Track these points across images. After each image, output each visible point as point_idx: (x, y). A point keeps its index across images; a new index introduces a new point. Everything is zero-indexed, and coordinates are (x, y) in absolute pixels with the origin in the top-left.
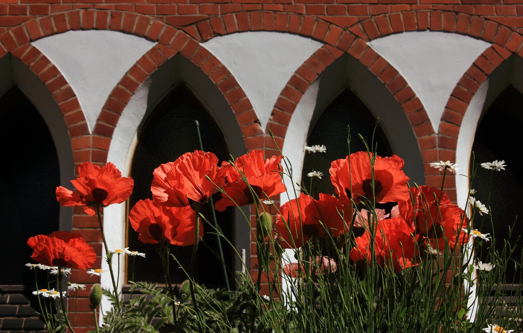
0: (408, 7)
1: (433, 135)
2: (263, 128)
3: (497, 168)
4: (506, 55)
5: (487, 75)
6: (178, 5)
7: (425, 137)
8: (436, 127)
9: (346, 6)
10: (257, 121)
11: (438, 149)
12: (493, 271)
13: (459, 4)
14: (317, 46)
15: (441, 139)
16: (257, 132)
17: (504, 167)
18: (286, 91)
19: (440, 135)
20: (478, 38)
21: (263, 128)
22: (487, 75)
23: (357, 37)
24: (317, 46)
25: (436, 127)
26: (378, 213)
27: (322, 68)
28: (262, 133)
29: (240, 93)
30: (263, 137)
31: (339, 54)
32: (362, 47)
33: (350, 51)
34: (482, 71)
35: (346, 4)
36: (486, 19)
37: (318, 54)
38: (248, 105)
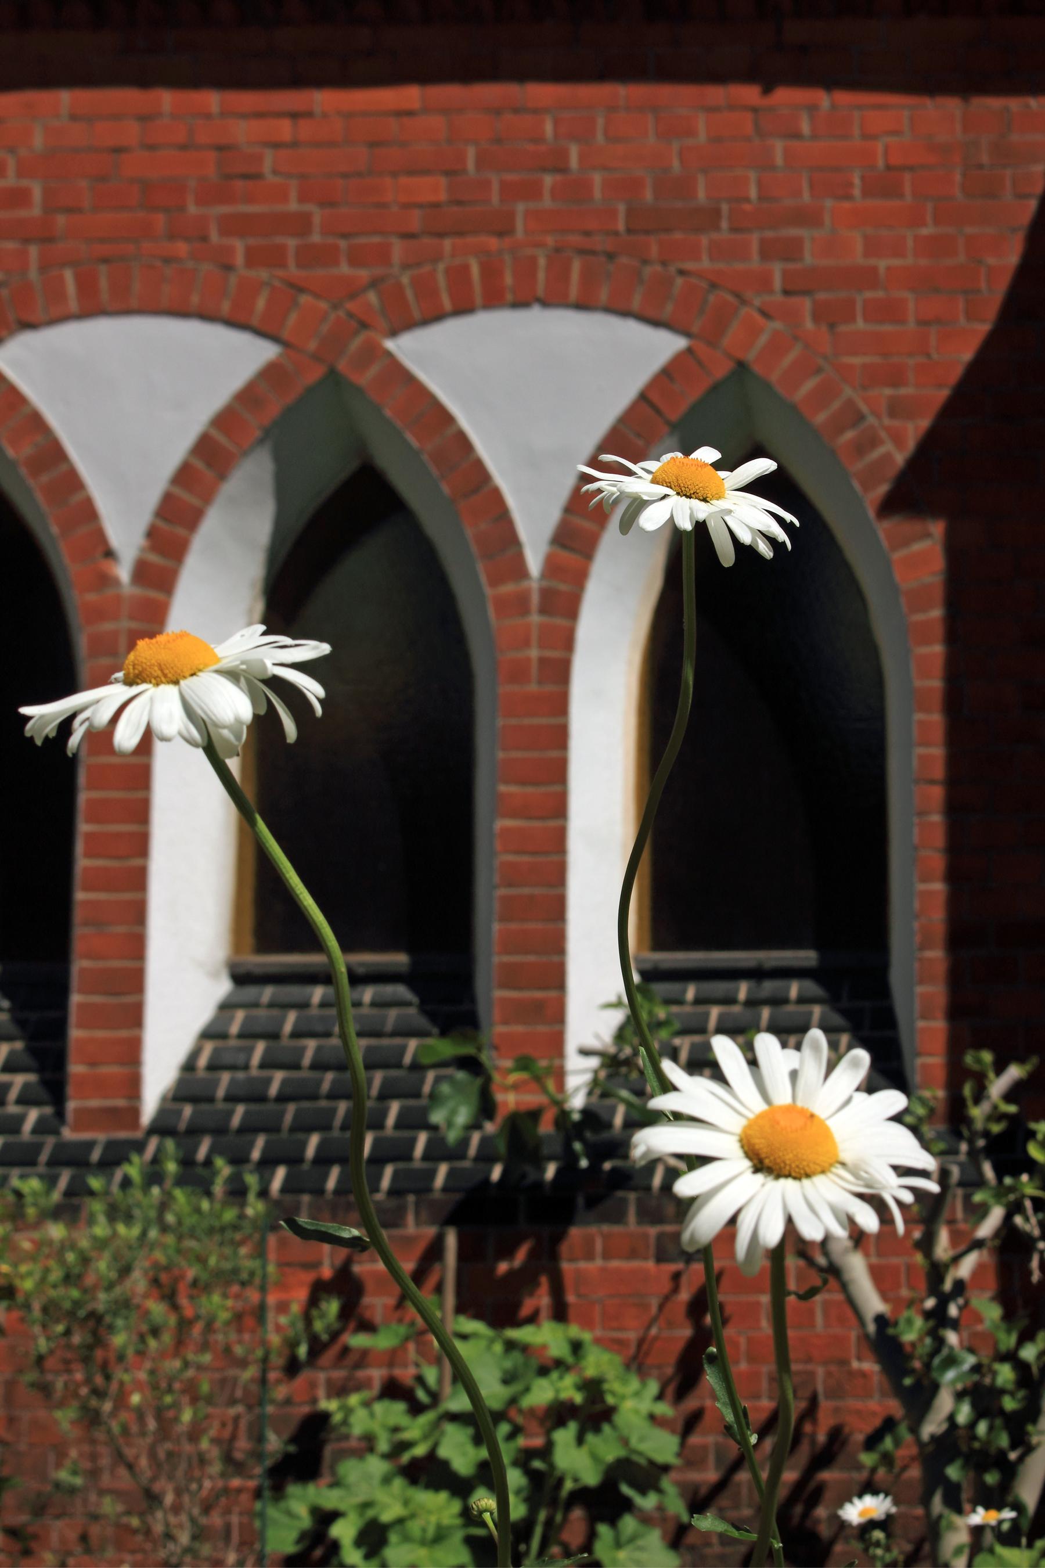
0: (493, 243)
1: (525, 584)
2: (123, 572)
3: (599, 1332)
4: (722, 369)
5: (668, 423)
6: (928, 355)
7: (508, 588)
8: (534, 561)
9: (343, 244)
10: (109, 554)
11: (535, 619)
12: (632, 1019)
13: (616, 233)
14: (264, 352)
15: (546, 594)
16: (106, 580)
17: (668, 1087)
18: (184, 476)
19: (545, 584)
20: (656, 323)
21: (123, 572)
22: (668, 423)
23: (364, 325)
24: (264, 352)
25: (534, 561)
26: (30, 1274)
27: (275, 406)
28: (116, 582)
29: (73, 482)
30: (118, 598)
31: (315, 374)
32: (374, 353)
33: (342, 365)
34: (658, 411)
35: (344, 236)
36: (682, 272)
37: (270, 373)
38: (89, 512)
